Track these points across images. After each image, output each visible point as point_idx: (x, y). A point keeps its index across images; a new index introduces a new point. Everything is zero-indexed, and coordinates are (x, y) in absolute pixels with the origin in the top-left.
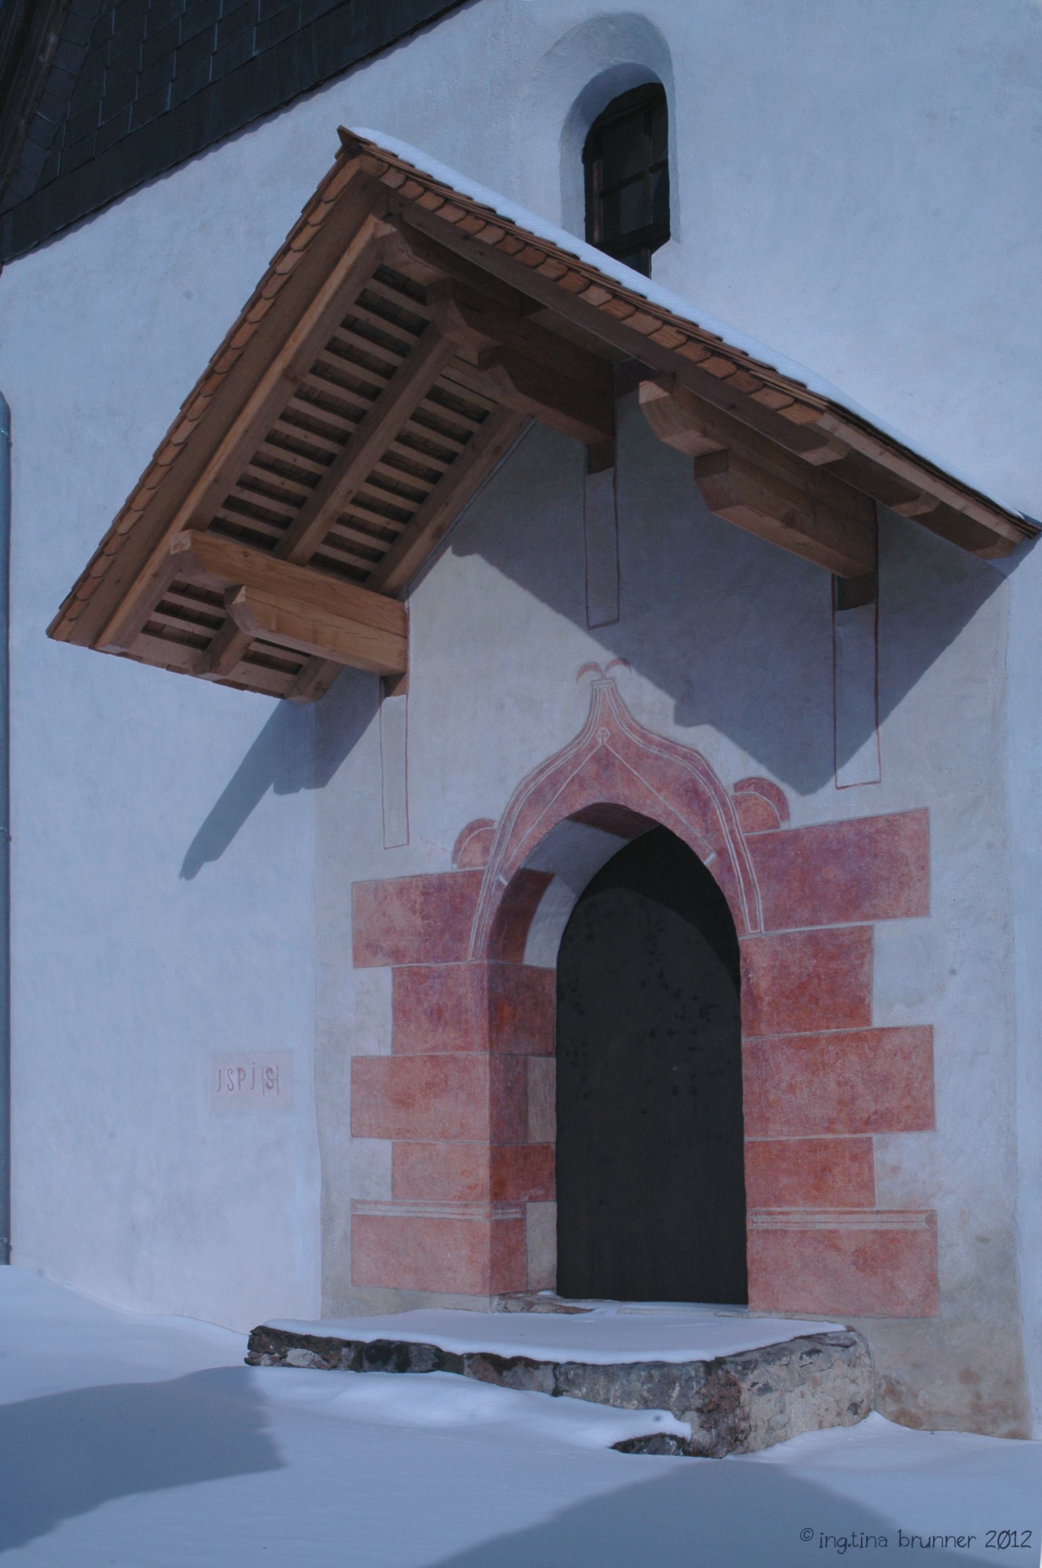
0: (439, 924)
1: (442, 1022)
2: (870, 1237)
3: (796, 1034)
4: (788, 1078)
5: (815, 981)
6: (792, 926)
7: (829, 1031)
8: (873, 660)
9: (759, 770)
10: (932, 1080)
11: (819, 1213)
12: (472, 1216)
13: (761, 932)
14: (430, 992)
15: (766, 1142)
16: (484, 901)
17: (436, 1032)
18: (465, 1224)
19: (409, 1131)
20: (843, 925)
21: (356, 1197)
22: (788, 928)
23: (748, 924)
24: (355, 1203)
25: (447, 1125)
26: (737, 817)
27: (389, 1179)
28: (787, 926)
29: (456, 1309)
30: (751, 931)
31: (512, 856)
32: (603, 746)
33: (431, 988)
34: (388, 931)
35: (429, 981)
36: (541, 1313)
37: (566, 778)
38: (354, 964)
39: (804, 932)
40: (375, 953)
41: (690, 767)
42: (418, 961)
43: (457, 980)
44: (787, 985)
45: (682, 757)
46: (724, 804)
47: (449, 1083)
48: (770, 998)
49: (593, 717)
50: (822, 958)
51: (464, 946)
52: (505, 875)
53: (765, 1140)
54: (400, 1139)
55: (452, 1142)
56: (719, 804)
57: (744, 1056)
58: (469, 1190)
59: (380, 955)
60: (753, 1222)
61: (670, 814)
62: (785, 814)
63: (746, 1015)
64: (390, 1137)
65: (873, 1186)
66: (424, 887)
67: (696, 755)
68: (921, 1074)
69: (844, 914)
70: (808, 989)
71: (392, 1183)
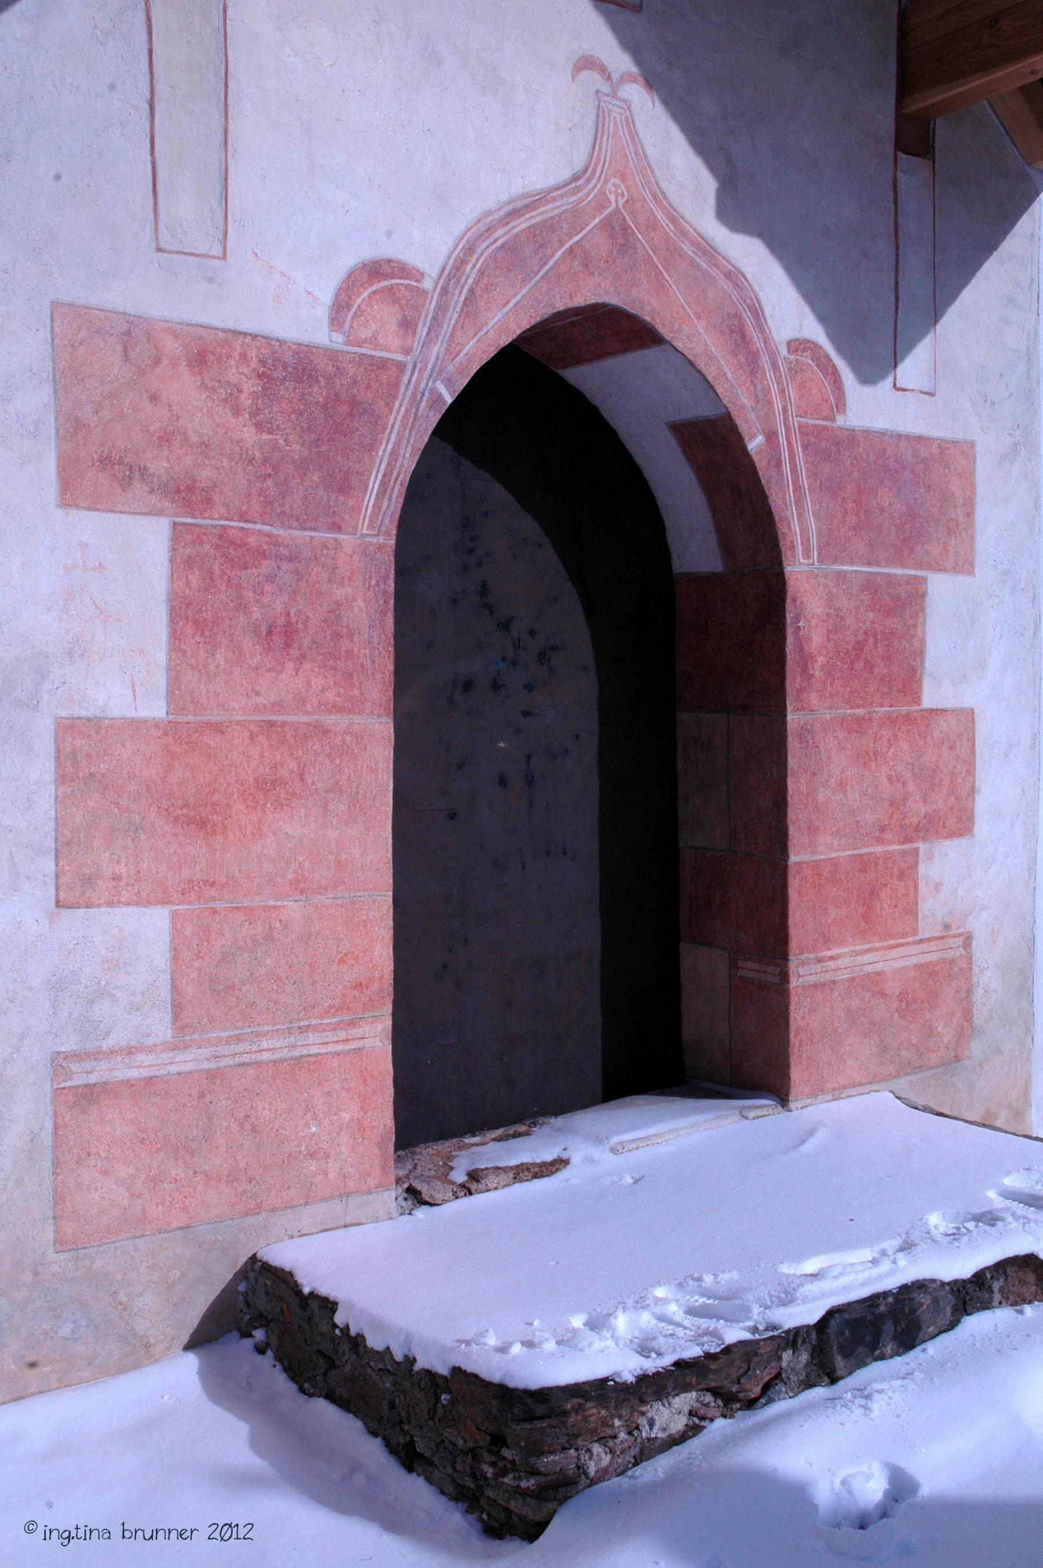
0: (297, 447)
1: (294, 653)
2: (912, 974)
4: (838, 773)
5: (871, 641)
8: (932, 236)
9: (815, 332)
10: (974, 776)
11: (867, 951)
12: (362, 1041)
13: (813, 564)
14: (268, 588)
15: (816, 861)
16: (404, 425)
17: (279, 672)
18: (348, 1059)
19: (213, 884)
20: (899, 571)
21: (70, 1045)
22: (844, 565)
23: (799, 550)
24: (59, 1062)
25: (307, 865)
26: (791, 392)
27: (165, 993)
29: (326, 1230)
30: (801, 560)
31: (465, 351)
32: (617, 211)
33: (271, 578)
34: (165, 439)
35: (265, 563)
36: (496, 1188)
37: (562, 243)
38: (62, 498)
39: (861, 572)
40: (126, 483)
41: (734, 295)
42: (243, 517)
43: (334, 569)
45: (724, 275)
46: (774, 365)
47: (309, 779)
49: (599, 155)
51: (351, 502)
52: (449, 383)
53: (814, 858)
54: (190, 903)
55: (316, 899)
56: (769, 364)
57: (790, 739)
58: (355, 992)
59: (139, 489)
60: (799, 976)
61: (711, 358)
62: (841, 405)
63: (793, 681)
64: (165, 902)
65: (917, 909)
66: (262, 362)
67: (741, 278)
68: (965, 768)
69: (899, 560)
71: (173, 1000)
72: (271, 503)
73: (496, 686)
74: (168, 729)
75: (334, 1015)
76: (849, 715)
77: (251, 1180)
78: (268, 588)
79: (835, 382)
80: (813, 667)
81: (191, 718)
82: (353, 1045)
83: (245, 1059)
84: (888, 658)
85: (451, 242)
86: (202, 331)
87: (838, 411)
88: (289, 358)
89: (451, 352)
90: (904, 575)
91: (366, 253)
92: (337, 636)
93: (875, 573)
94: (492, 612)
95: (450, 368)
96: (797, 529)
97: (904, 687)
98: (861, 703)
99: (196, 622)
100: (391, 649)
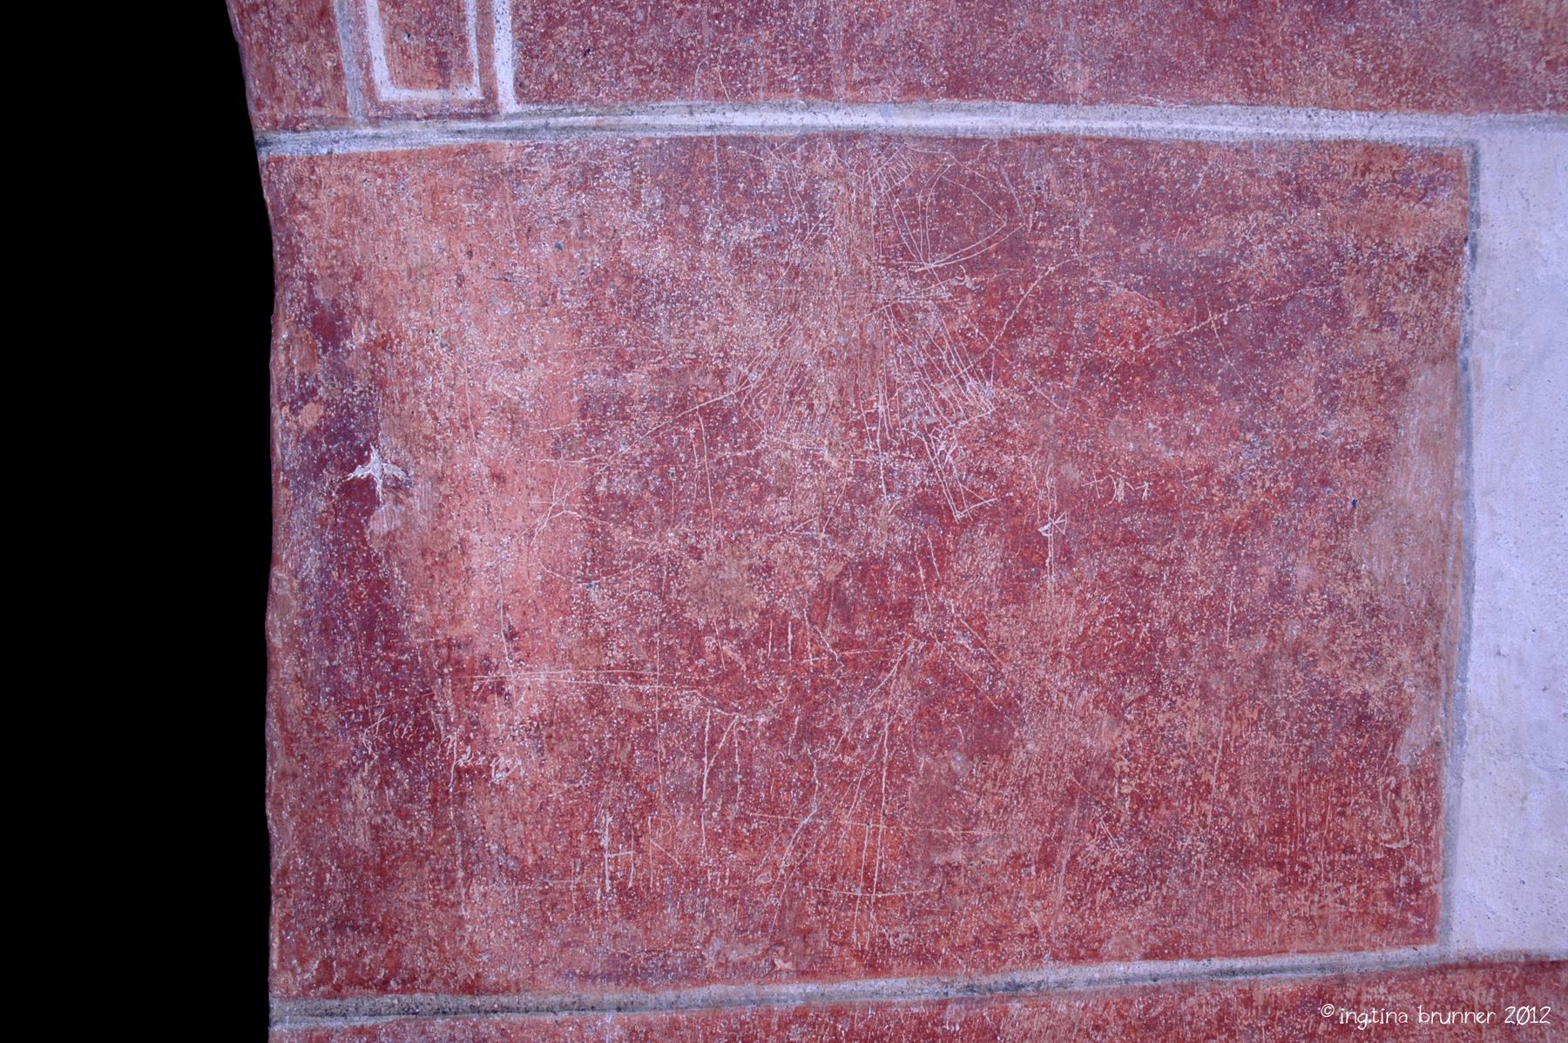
3: (794, 992)
6: (776, 85)
7: (1093, 971)
13: (487, 107)
28: (737, 89)
39: (889, 141)
44: (731, 572)
48: (565, 676)
50: (1055, 369)
70: (922, 620)
76: (801, 1015)
80: (475, 731)
90: (1268, 147)
98: (903, 934)
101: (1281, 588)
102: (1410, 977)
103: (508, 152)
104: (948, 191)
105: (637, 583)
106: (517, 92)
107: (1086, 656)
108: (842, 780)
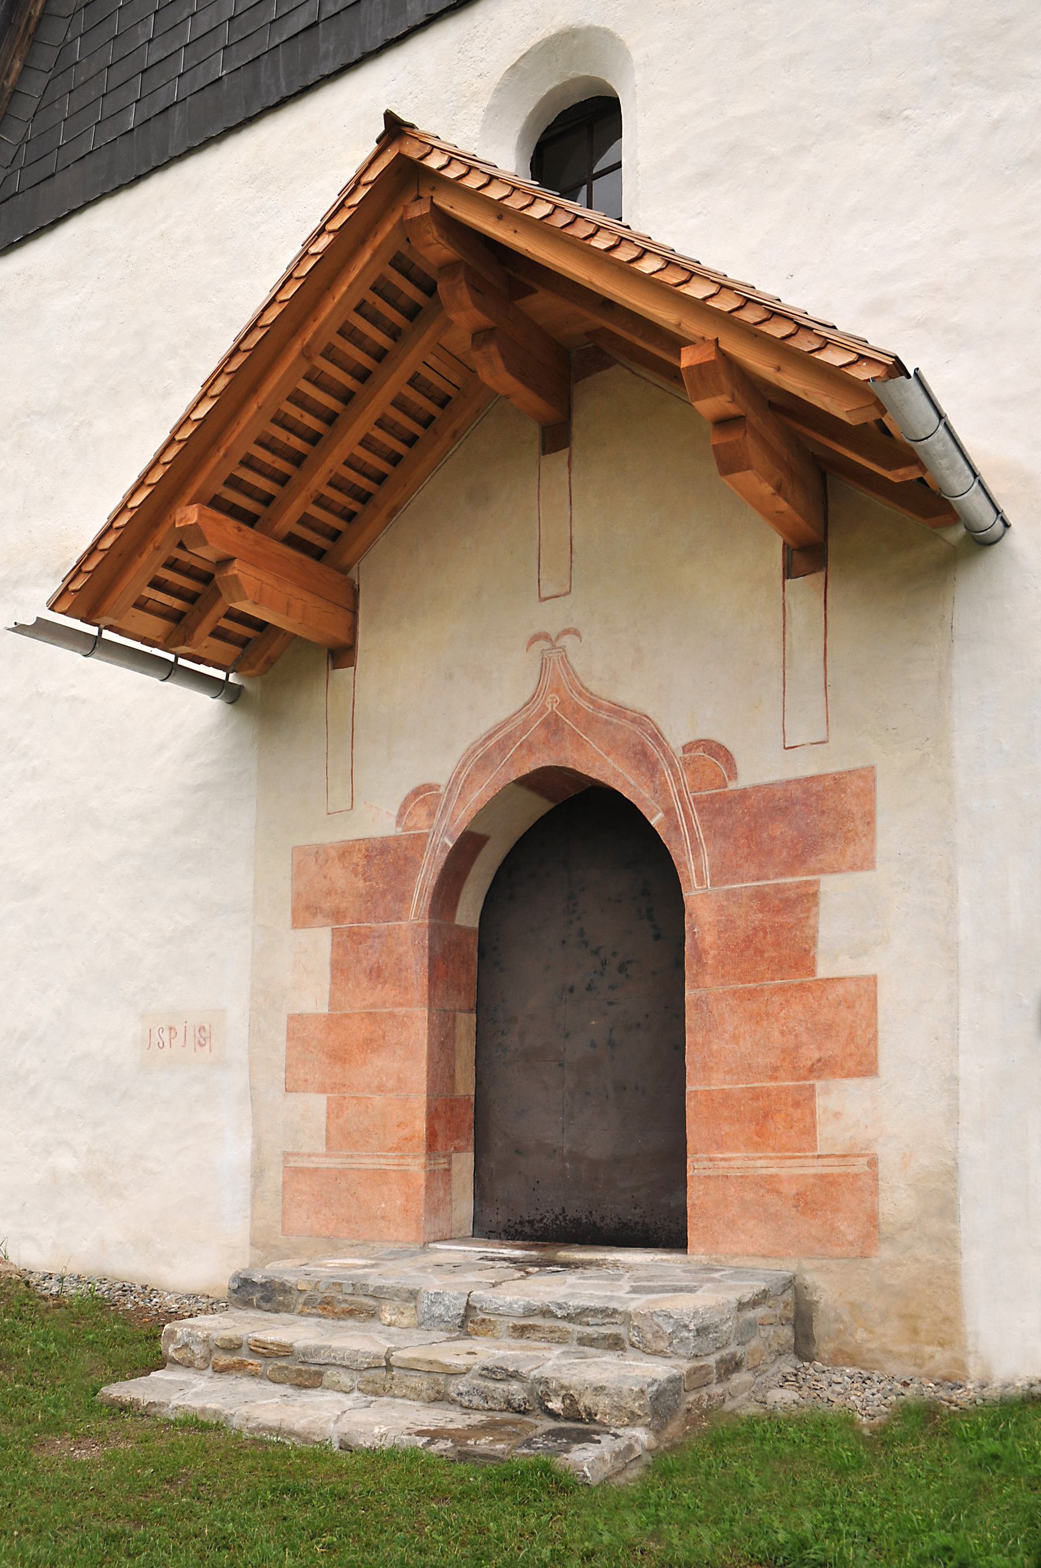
1: (381, 980)
2: (812, 1180)
3: (741, 986)
4: (731, 1029)
13: (707, 888)
14: (370, 951)
20: (789, 880)
21: (289, 1149)
22: (734, 884)
24: (286, 1155)
28: (733, 883)
32: (553, 712)
33: (371, 947)
40: (315, 915)
46: (672, 765)
47: (387, 1038)
50: (769, 911)
51: (406, 906)
52: (451, 837)
55: (389, 1095)
59: (319, 917)
62: (733, 774)
64: (324, 1092)
66: (367, 850)
69: (790, 868)
72: (370, 913)
73: (589, 988)
74: (330, 1018)
75: (394, 1152)
77: (356, 1223)
78: (370, 951)
79: (727, 760)
80: (706, 959)
81: (338, 1012)
82: (403, 1168)
83: (354, 1166)
84: (777, 945)
85: (455, 764)
86: (343, 844)
87: (730, 779)
88: (378, 846)
89: (452, 820)
91: (415, 784)
92: (400, 970)
93: (763, 886)
94: (587, 946)
95: (452, 829)
96: (693, 867)
97: (796, 964)
99: (341, 970)
100: (426, 974)
101: (795, 935)
102: (812, 981)
103: (709, 893)
104: (757, 892)
105: (723, 941)
106: (862, 868)
107: (773, 945)
108: (745, 961)
